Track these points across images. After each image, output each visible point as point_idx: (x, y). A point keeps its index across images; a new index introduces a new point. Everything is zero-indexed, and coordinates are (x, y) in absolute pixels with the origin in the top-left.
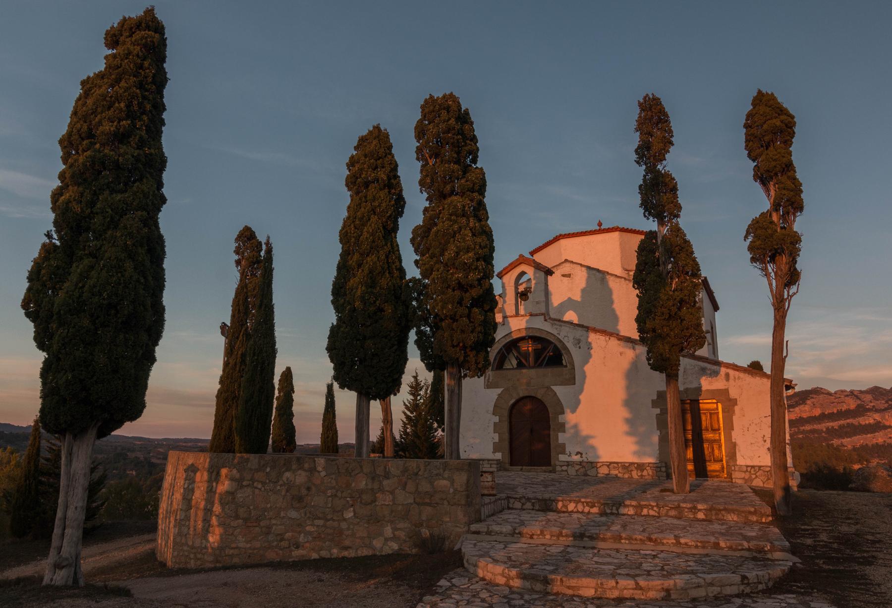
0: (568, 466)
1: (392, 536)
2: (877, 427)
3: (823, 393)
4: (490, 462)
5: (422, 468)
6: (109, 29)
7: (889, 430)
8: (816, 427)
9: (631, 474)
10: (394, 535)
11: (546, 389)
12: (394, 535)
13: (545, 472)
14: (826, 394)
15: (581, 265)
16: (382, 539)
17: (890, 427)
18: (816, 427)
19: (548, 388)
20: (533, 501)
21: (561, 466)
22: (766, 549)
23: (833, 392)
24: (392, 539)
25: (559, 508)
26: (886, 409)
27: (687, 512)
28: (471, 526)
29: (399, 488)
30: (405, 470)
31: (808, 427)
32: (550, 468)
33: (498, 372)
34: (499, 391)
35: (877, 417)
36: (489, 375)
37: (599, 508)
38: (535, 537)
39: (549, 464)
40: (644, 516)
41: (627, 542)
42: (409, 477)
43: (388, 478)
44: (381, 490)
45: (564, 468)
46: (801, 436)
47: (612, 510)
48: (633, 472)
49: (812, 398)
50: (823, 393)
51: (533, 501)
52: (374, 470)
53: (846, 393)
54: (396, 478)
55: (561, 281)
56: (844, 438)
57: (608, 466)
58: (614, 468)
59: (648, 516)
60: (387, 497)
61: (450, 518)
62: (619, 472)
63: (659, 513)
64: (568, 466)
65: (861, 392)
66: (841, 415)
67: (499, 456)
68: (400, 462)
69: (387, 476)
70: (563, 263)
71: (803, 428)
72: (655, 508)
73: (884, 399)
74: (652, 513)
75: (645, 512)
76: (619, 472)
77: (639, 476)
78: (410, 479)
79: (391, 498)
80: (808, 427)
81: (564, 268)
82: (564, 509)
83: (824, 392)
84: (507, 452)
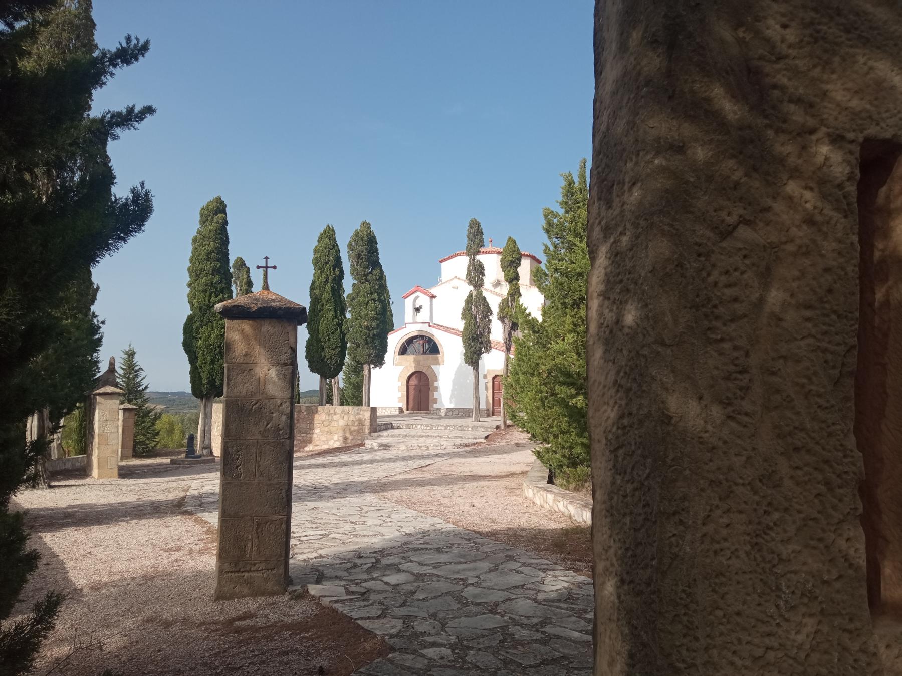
6: (110, 165)
19: (429, 366)
24: (337, 441)
30: (343, 411)
32: (429, 412)
33: (403, 356)
34: (402, 367)
38: (430, 448)
39: (428, 409)
45: (435, 411)
61: (350, 429)
68: (341, 407)
69: (335, 414)
70: (452, 280)
75: (449, 428)
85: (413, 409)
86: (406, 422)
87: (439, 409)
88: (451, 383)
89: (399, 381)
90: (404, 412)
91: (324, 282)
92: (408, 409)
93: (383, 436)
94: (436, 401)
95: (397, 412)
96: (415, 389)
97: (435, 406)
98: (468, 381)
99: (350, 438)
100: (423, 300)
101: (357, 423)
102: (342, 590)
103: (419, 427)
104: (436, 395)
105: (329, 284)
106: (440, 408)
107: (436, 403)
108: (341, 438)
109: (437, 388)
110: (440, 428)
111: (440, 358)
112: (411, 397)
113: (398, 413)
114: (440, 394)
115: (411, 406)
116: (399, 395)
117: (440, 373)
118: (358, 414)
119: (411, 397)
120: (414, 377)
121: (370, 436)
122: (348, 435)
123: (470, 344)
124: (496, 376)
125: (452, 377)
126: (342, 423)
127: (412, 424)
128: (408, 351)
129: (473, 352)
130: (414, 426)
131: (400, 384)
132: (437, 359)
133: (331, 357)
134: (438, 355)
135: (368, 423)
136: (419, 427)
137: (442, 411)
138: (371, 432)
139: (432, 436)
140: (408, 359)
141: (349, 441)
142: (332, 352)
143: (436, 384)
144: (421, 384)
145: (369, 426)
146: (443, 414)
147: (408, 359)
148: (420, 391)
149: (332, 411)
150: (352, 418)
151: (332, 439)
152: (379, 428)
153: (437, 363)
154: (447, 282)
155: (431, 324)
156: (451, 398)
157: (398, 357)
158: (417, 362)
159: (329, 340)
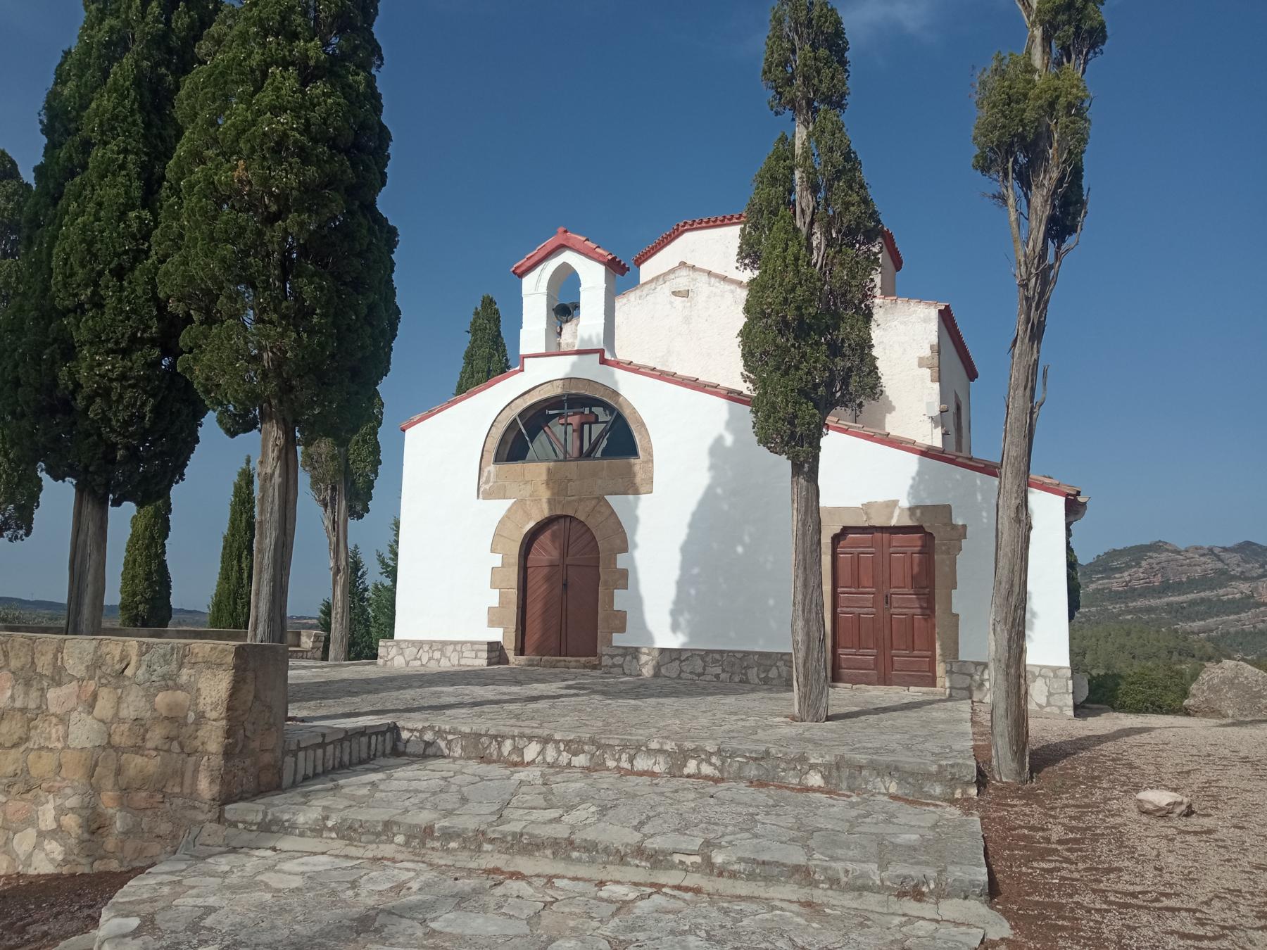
0: (624, 655)
1: (54, 826)
2: (1247, 603)
3: (1167, 550)
4: (476, 647)
5: (134, 659)
7: (1262, 609)
8: (1154, 602)
9: (746, 674)
10: (60, 826)
11: (594, 502)
12: (60, 826)
13: (585, 667)
14: (1172, 552)
15: (709, 273)
16: (31, 833)
17: (1264, 604)
18: (1154, 602)
19: (601, 500)
20: (450, 737)
21: (612, 657)
22: (925, 889)
23: (1182, 547)
25: (506, 754)
26: (1260, 577)
27: (784, 770)
28: (228, 807)
29: (80, 709)
30: (96, 664)
31: (1141, 603)
33: (516, 466)
34: (508, 503)
35: (1245, 587)
36: (489, 472)
37: (593, 755)
39: (593, 652)
40: (689, 776)
41: (585, 856)
42: (103, 681)
43: (59, 684)
44: (42, 711)
45: (618, 660)
46: (1129, 617)
47: (619, 760)
48: (749, 671)
49: (1151, 557)
50: (1167, 550)
51: (450, 737)
52: (33, 662)
53: (1201, 552)
54: (75, 683)
55: (671, 303)
56: (1194, 621)
57: (702, 658)
58: (715, 661)
59: (697, 776)
60: (54, 731)
62: (723, 671)
63: (721, 771)
64: (624, 655)
65: (1225, 549)
66: (1192, 584)
67: (497, 635)
70: (673, 271)
71: (1134, 604)
72: (714, 760)
73: (1257, 561)
74: (706, 769)
75: (691, 767)
76: (723, 671)
77: (760, 679)
78: (105, 686)
79: (61, 732)
80: (1141, 603)
81: (678, 280)
82: (515, 758)
83: (1170, 548)
84: (513, 627)
85: (540, 650)
86: (465, 722)
87: (634, 652)
88: (677, 558)
89: (493, 551)
90: (507, 662)
91: (107, 45)
92: (520, 650)
93: (287, 829)
94: (619, 620)
95: (481, 662)
96: (548, 578)
97: (619, 640)
98: (740, 549)
99: (119, 825)
100: (592, 276)
101: (156, 736)
102: (542, 801)
103: (531, 751)
104: (620, 600)
105: (128, 60)
106: (637, 649)
107: (622, 629)
108: (71, 821)
109: (624, 574)
110: (642, 763)
111: (637, 468)
112: (535, 609)
113: (485, 662)
114: (638, 601)
115: (533, 637)
116: (493, 598)
117: (635, 520)
118: (170, 682)
119: (535, 609)
120: (545, 538)
121: (220, 819)
122: (108, 802)
123: (786, 351)
124: (846, 530)
125: (681, 534)
126: (84, 732)
127: (499, 738)
128: (531, 454)
129: (801, 392)
130: (508, 745)
131: (497, 560)
132: (629, 473)
133: (105, 393)
134: (632, 460)
135: (212, 739)
136: (531, 751)
137: (644, 659)
138: (226, 799)
139: (590, 847)
140: (528, 477)
141: (110, 844)
142: (111, 365)
143: (621, 561)
144: (569, 561)
145: (218, 761)
146: (647, 672)
147: (528, 477)
148: (565, 585)
149: (44, 664)
150: (134, 705)
151: (31, 821)
152: (304, 763)
153: (631, 487)
154: (657, 278)
155: (607, 356)
156: (675, 613)
157: (491, 468)
158: (557, 484)
159: (98, 304)
